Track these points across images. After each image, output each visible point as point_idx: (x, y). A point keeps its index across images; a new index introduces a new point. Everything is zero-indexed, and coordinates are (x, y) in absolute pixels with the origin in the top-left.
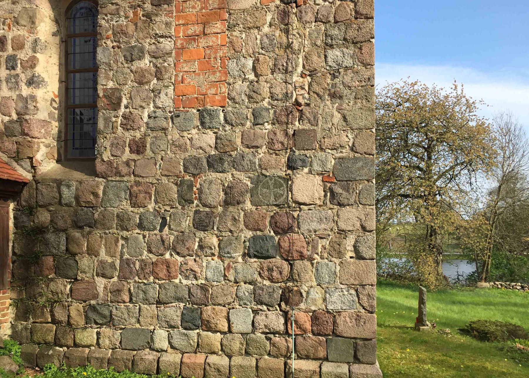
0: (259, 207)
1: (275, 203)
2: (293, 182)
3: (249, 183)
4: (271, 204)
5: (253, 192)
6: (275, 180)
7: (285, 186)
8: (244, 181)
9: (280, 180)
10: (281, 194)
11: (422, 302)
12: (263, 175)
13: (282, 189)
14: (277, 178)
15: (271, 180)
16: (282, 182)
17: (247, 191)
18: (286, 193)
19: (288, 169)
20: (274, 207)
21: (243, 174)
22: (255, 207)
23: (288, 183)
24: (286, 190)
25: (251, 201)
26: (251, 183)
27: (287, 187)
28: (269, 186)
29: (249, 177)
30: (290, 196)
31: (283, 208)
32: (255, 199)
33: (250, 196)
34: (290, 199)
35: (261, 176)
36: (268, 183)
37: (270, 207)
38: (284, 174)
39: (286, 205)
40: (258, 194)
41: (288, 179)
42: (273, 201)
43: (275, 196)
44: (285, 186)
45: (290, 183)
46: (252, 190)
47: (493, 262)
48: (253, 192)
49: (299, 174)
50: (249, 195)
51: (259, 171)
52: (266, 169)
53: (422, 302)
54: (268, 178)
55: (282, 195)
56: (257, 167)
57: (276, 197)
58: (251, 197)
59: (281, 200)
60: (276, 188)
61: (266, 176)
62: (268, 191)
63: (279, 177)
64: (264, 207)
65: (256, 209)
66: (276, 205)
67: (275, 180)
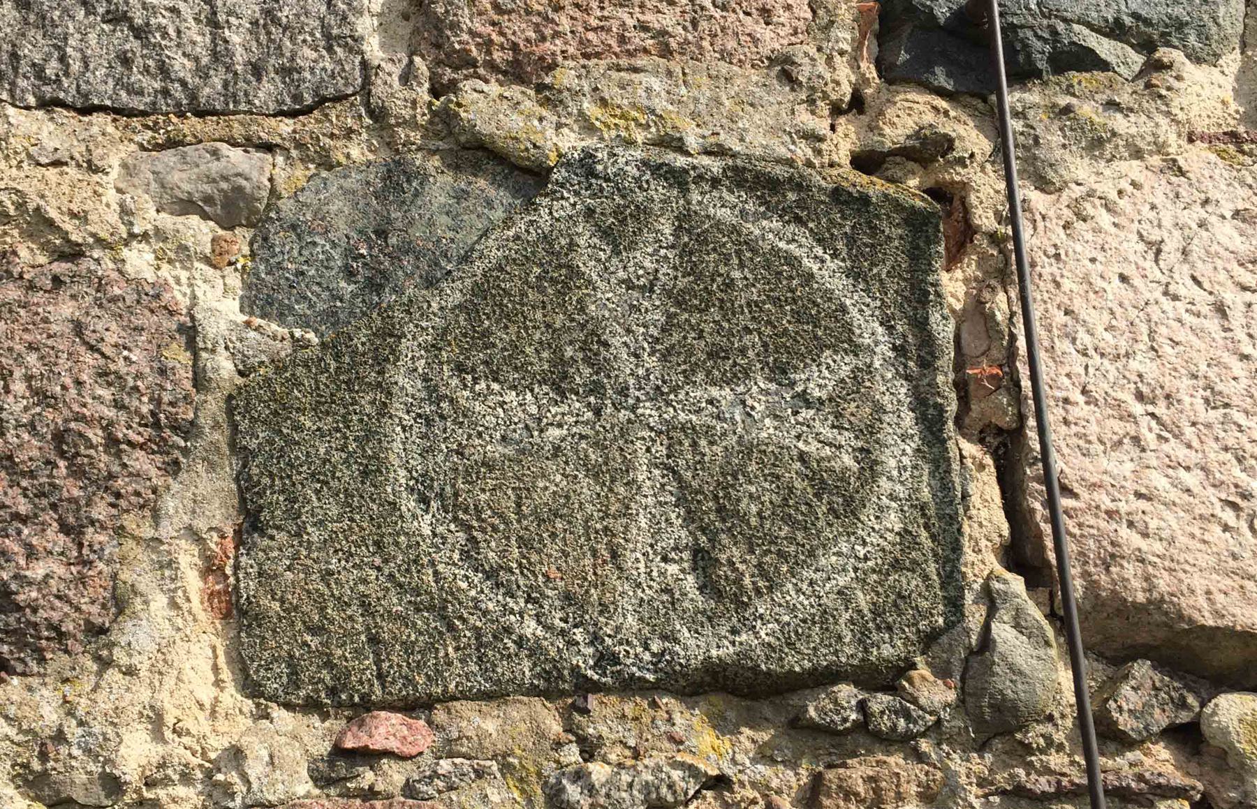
0: (387, 730)
1: (698, 646)
2: (1008, 266)
3: (220, 303)
4: (637, 660)
5: (285, 444)
6: (693, 236)
7: (870, 330)
8: (139, 260)
9: (769, 231)
10: (821, 480)
11: (1090, 770)
12: (477, 154)
13: (818, 380)
14: (722, 208)
15: (613, 239)
16: (829, 274)
17: (169, 435)
18: (899, 450)
19: (891, 75)
20: (687, 719)
21: (116, 146)
22: (317, 735)
23: (920, 296)
24: (893, 393)
25: (235, 612)
26: (260, 301)
27: (917, 351)
28: (593, 342)
29: (231, 207)
30: (986, 516)
31: (867, 735)
32: (311, 564)
33: (219, 515)
34: (981, 562)
35: (441, 185)
36: (565, 277)
37: (604, 720)
38: (844, 141)
39: (934, 693)
40: (372, 470)
41: (918, 224)
42: (661, 613)
43: (709, 513)
44: (870, 330)
45: (953, 286)
46: (260, 404)
47: (96, 471)
48: (285, 444)
49: (1096, 144)
50: (200, 499)
51: (407, 99)
52: (522, 70)
53: (1090, 770)
54: (559, 210)
55: (844, 498)
56: (373, 48)
57: (730, 527)
58: (251, 523)
59: (823, 592)
60: (722, 362)
61: (528, 176)
62: (566, 419)
63: (754, 180)
64: (483, 723)
65: (339, 765)
66: (734, 690)
67: (693, 236)
